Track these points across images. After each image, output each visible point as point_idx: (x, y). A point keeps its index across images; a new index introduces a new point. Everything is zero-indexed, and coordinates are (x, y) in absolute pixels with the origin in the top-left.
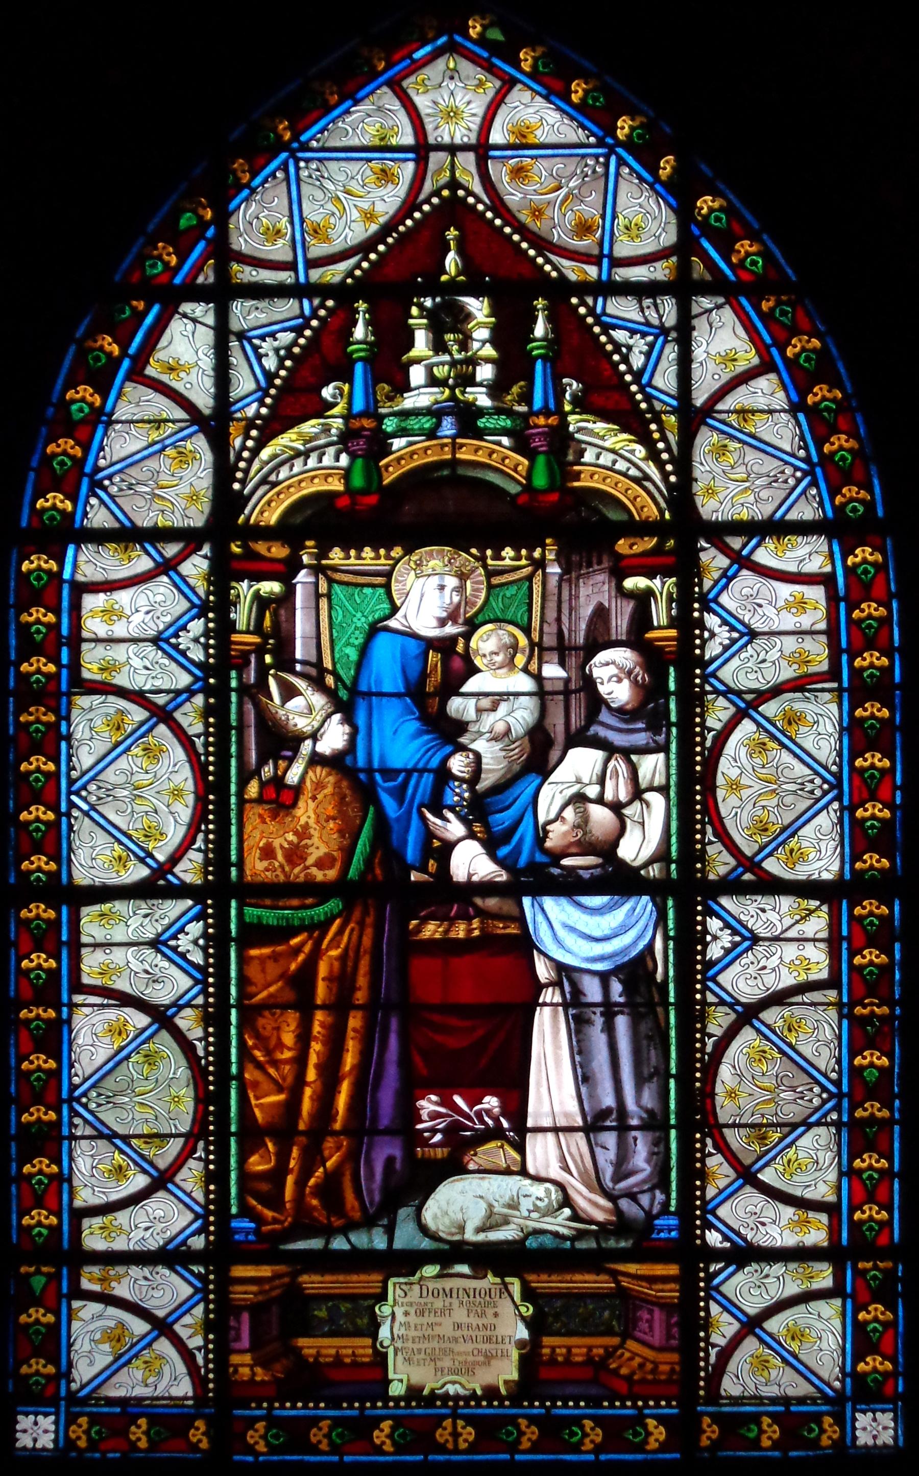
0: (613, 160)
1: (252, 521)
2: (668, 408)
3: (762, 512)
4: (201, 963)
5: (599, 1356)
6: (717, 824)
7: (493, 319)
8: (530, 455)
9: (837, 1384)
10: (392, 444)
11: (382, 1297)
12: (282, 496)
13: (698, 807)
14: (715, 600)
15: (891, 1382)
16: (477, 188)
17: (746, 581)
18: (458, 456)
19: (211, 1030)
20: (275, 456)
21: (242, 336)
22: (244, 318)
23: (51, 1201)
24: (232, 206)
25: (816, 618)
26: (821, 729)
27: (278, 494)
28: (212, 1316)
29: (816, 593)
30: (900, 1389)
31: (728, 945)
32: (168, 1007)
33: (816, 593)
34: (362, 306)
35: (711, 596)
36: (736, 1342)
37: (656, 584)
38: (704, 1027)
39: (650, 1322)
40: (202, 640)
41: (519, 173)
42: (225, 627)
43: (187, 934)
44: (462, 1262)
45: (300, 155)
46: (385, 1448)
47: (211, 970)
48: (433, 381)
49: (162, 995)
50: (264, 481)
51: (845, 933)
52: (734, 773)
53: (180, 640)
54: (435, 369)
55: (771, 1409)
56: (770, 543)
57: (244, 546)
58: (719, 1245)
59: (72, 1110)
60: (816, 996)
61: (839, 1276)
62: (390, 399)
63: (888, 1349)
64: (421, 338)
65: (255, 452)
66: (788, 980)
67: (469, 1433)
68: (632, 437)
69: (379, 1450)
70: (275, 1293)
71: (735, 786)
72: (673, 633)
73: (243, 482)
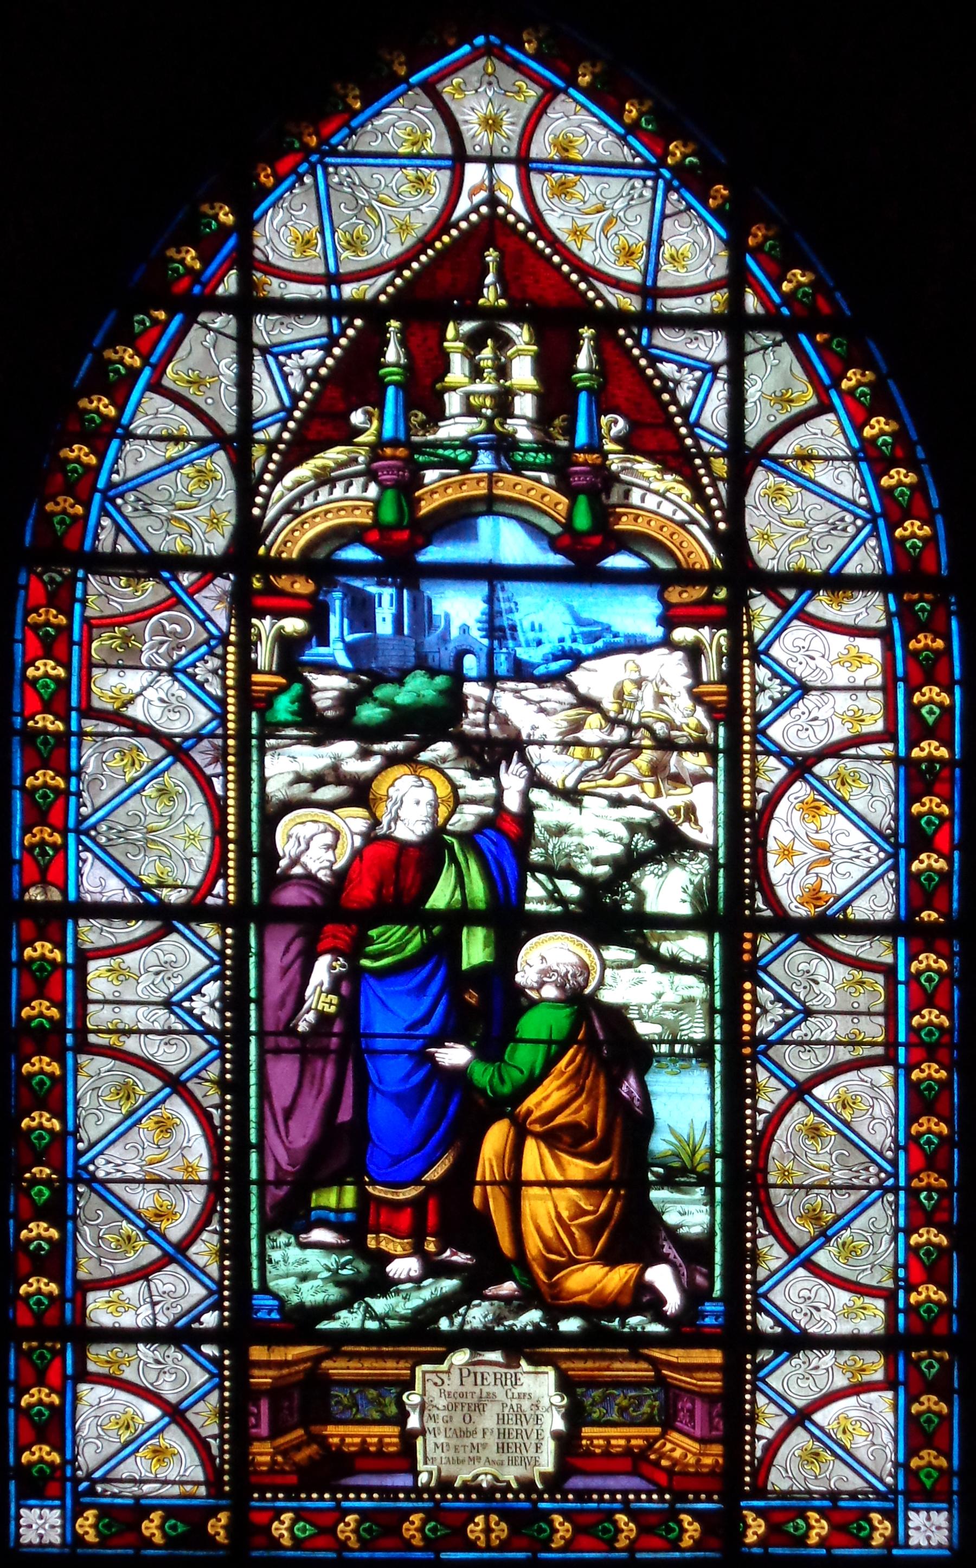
0: (661, 184)
1: (272, 554)
2: (717, 450)
3: (818, 563)
4: (218, 1027)
5: (638, 1447)
6: (769, 1217)
7: (535, 348)
8: (571, 492)
9: (889, 1480)
10: (424, 476)
11: (409, 1385)
12: (306, 526)
13: (747, 850)
14: (766, 652)
15: (943, 1321)
16: (518, 205)
17: (798, 633)
18: (495, 491)
19: (228, 1097)
20: (299, 483)
21: (265, 350)
22: (268, 333)
23: (55, 817)
24: (256, 214)
25: (872, 673)
26: (877, 1112)
27: (303, 523)
28: (226, 1324)
29: (873, 647)
30: (955, 1328)
31: (777, 696)
32: (186, 737)
33: (873, 647)
34: (394, 324)
35: (762, 647)
36: (783, 1109)
37: (705, 632)
38: (755, 1102)
39: (691, 1412)
40: (220, 672)
41: (562, 190)
42: (247, 666)
43: (204, 995)
44: (492, 1349)
45: (329, 160)
46: (414, 1542)
47: (227, 1362)
48: (471, 411)
49: (177, 725)
50: (287, 509)
51: (901, 1377)
52: (786, 839)
53: (197, 670)
54: (471, 398)
55: (817, 1503)
56: (822, 595)
57: (267, 582)
58: (769, 1330)
59: (80, 842)
60: (873, 749)
61: (891, 1368)
62: (423, 426)
63: (944, 845)
64: (458, 371)
65: (279, 476)
66: (841, 733)
67: (501, 1530)
68: (679, 478)
69: (408, 1545)
70: (296, 1378)
71: (787, 853)
72: (723, 688)
73: (264, 508)
